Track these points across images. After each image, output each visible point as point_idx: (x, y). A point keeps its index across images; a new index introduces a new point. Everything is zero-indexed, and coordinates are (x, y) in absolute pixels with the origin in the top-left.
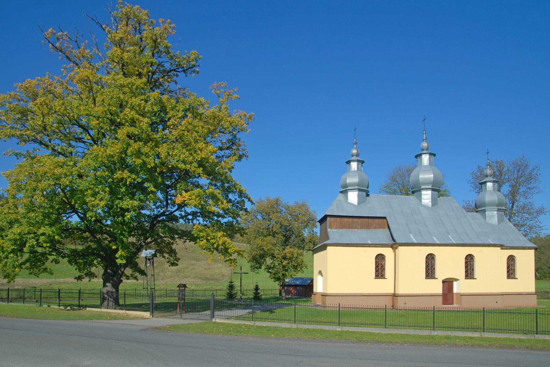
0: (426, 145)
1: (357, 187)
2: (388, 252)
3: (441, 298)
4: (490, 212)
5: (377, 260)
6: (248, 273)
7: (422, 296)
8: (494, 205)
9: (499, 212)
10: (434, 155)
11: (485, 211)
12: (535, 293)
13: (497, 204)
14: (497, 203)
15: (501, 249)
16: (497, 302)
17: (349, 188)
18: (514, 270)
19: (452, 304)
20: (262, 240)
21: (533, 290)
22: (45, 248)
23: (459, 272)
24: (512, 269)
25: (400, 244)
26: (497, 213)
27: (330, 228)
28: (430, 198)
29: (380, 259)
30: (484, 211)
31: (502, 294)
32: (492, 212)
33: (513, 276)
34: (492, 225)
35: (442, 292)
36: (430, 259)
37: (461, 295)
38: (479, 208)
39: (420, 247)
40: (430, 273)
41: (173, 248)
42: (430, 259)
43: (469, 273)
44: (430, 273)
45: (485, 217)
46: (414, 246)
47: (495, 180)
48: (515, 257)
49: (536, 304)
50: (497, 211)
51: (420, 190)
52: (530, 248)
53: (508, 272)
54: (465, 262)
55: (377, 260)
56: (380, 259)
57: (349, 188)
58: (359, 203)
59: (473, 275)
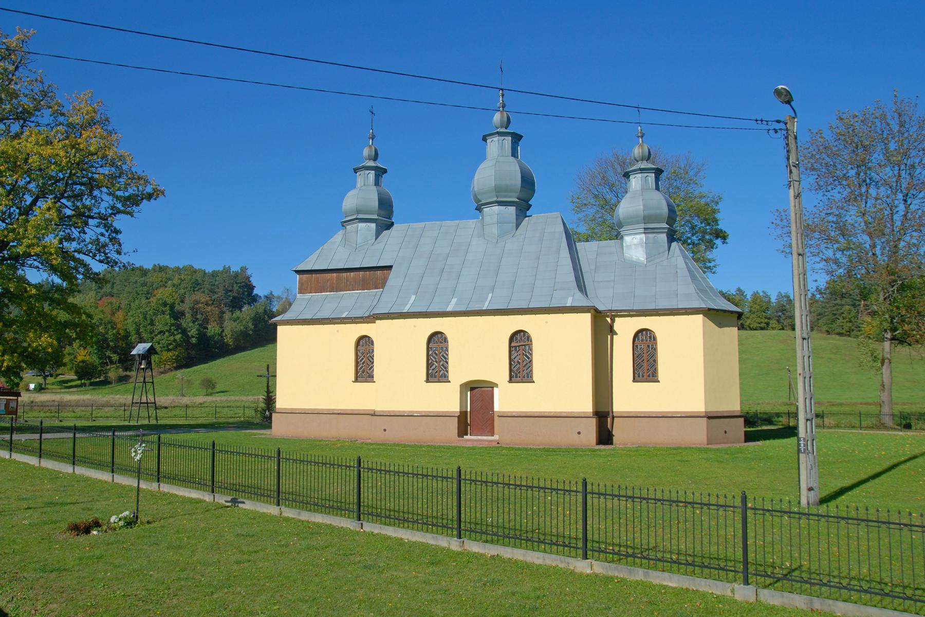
3: (454, 422)
6: (268, 366)
7: (410, 415)
13: (644, 217)
14: (642, 214)
16: (579, 433)
19: (493, 435)
22: (828, 315)
25: (423, 315)
27: (300, 293)
34: (633, 266)
35: (458, 410)
36: (437, 342)
39: (561, 315)
41: (209, 334)
42: (437, 342)
46: (417, 318)
49: (705, 441)
50: (645, 233)
58: (649, 257)
59: (531, 377)
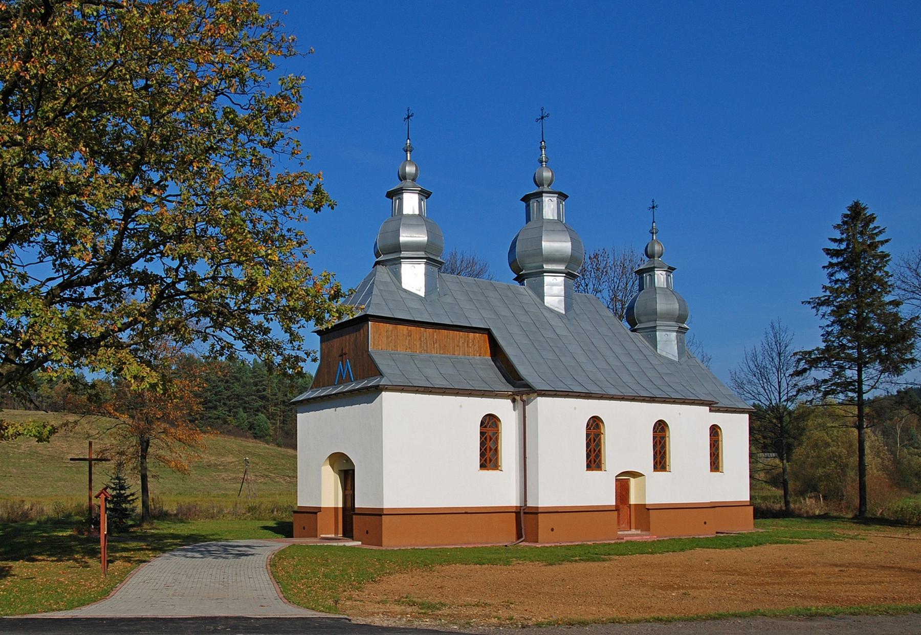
0: (550, 174)
1: (422, 254)
2: (503, 409)
4: (664, 333)
5: (485, 430)
8: (671, 319)
9: (679, 334)
10: (566, 197)
11: (656, 331)
12: (749, 504)
15: (711, 411)
17: (404, 254)
18: (496, 450)
20: (240, 372)
21: (746, 497)
23: (644, 460)
24: (491, 450)
26: (677, 336)
28: (563, 293)
29: (490, 425)
30: (654, 329)
31: (714, 506)
32: (667, 333)
33: (713, 470)
37: (648, 509)
38: (640, 322)
40: (594, 460)
43: (660, 462)
44: (594, 460)
45: (654, 342)
47: (813, 306)
48: (603, 422)
50: (677, 332)
51: (541, 273)
52: (742, 411)
53: (482, 455)
54: (481, 433)
55: (485, 430)
56: (490, 425)
57: (404, 254)
